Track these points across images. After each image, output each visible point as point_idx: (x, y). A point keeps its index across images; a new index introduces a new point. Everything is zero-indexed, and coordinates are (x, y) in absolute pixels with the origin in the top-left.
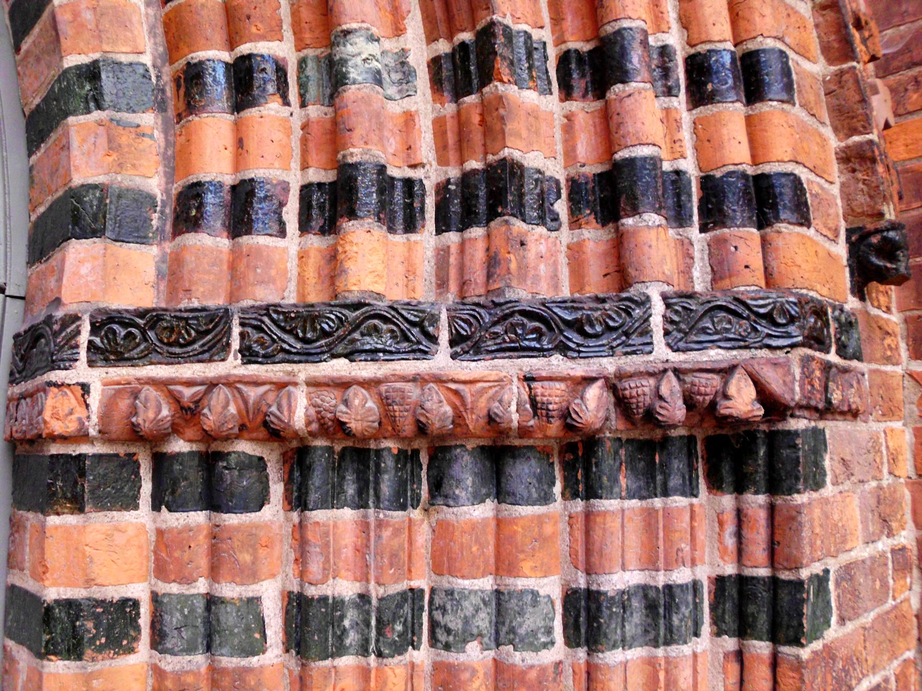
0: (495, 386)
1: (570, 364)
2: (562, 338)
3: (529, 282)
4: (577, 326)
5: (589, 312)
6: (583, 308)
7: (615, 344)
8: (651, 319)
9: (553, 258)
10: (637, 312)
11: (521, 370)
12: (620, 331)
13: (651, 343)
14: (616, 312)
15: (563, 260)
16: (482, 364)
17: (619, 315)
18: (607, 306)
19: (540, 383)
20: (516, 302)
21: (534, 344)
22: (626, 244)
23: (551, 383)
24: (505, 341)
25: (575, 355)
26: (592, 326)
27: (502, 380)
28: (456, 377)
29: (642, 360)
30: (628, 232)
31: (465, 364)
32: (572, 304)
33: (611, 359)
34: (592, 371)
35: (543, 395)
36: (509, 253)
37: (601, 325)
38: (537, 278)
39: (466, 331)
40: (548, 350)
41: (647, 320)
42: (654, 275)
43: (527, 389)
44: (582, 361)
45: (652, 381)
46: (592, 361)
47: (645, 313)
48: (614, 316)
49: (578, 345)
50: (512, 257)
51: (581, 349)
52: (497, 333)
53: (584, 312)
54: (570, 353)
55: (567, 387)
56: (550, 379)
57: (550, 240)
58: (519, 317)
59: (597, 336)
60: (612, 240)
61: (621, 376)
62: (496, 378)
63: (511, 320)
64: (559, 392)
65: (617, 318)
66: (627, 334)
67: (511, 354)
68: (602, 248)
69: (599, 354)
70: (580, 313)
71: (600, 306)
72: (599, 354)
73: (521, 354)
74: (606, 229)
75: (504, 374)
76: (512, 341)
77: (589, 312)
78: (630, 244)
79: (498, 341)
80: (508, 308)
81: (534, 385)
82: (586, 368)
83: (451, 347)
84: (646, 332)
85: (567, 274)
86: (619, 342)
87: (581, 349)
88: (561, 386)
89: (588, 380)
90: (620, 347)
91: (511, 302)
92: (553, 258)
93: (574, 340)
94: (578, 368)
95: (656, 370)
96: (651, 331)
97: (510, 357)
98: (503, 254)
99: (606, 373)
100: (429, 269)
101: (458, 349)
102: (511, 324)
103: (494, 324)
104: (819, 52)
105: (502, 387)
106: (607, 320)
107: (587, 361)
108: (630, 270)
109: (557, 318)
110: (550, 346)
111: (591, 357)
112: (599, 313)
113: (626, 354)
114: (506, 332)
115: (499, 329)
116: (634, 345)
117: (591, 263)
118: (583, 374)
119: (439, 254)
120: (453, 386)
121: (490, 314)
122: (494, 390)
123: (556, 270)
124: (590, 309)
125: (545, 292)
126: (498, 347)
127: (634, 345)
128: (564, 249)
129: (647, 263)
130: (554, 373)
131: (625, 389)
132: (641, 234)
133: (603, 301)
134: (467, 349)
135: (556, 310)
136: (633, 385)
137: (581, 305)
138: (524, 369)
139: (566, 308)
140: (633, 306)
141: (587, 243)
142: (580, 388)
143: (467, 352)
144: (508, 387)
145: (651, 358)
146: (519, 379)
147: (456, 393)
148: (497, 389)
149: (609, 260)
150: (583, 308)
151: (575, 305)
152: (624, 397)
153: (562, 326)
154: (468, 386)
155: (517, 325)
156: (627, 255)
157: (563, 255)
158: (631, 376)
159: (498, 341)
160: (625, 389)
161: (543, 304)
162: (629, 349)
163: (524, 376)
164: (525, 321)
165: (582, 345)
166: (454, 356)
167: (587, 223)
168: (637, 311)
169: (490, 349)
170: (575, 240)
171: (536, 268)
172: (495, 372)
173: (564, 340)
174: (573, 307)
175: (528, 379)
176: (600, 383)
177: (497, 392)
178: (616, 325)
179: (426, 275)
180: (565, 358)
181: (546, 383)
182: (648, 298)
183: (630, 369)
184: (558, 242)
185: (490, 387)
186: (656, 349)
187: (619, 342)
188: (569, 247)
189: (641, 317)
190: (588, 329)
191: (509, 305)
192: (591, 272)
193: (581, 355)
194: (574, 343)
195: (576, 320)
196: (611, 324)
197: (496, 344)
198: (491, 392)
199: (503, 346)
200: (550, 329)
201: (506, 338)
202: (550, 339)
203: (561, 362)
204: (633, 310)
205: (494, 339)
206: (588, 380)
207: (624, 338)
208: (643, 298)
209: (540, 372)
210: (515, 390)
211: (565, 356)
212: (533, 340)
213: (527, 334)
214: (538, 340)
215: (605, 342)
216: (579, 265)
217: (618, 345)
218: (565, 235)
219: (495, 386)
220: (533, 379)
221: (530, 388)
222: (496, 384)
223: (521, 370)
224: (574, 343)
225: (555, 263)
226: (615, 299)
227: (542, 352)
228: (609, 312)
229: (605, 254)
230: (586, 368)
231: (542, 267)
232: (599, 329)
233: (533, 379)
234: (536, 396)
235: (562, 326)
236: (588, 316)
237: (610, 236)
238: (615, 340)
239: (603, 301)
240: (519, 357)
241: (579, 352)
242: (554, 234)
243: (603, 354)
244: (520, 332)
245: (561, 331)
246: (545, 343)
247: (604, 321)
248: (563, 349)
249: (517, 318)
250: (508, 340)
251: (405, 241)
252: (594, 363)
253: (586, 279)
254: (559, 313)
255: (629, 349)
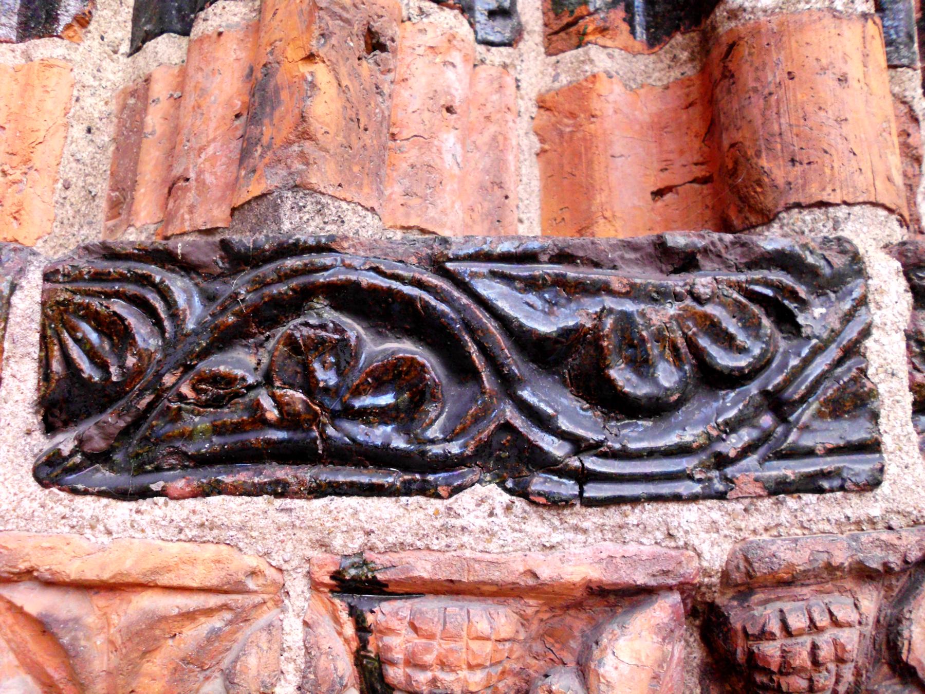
0: (209, 612)
1: (539, 526)
2: (510, 414)
3: (395, 190)
4: (576, 361)
5: (629, 306)
6: (604, 289)
7: (732, 444)
8: (869, 343)
9: (492, 129)
10: (817, 317)
11: (324, 545)
12: (753, 388)
13: (871, 447)
14: (739, 311)
15: (523, 139)
16: (154, 510)
17: (751, 326)
18: (703, 283)
19: (403, 607)
20: (320, 248)
21: (380, 434)
22: (748, 77)
23: (454, 608)
24: (259, 420)
25: (569, 488)
26: (641, 365)
27: (238, 589)
28: (46, 564)
29: (836, 514)
30: (756, 31)
31: (88, 506)
32: (557, 269)
33: (712, 510)
34: (633, 561)
35: (412, 662)
36: (310, 58)
37: (678, 359)
38: (427, 176)
39: (103, 366)
40: (447, 463)
41: (852, 350)
42: (861, 181)
43: (349, 630)
44: (592, 518)
45: (870, 601)
46: (634, 515)
47: (848, 318)
48: (732, 326)
49: (579, 446)
50: (321, 74)
51: (592, 463)
52: (228, 380)
53: (609, 302)
54: (539, 483)
55: (525, 620)
56: (451, 589)
57: (483, 72)
58: (330, 315)
59: (657, 409)
60: (684, 82)
61: (749, 579)
62: (213, 580)
63: (293, 326)
64: (488, 646)
65: (741, 338)
66: (778, 404)
67: (284, 473)
68: (648, 108)
69: (665, 489)
70: (592, 306)
71: (676, 283)
72: (665, 489)
73: (327, 474)
74: (664, 53)
75: (252, 561)
76: (289, 419)
77: (629, 306)
78: (761, 73)
79: (230, 415)
80: (283, 277)
81: (385, 613)
82: (611, 548)
83: (50, 428)
84: (856, 401)
85: (536, 185)
86: (746, 435)
87: (592, 463)
88: (496, 621)
89: (616, 598)
90: (752, 460)
91: (297, 249)
92: (492, 129)
93: (564, 424)
94: (577, 548)
95: (895, 561)
96: (873, 394)
97: (279, 490)
98: (293, 68)
99: (690, 569)
100: (86, 152)
101: (66, 442)
102: (290, 341)
103: (223, 339)
104: (561, 325)
105: (242, 617)
106: (704, 342)
107: (613, 516)
108: (764, 162)
109: (492, 325)
110: (454, 448)
111: (634, 501)
112: (672, 309)
113: (780, 489)
114: (268, 380)
115: (241, 363)
116: (810, 453)
117: (617, 149)
118: (596, 574)
119: (124, 107)
120: (33, 600)
121: (209, 298)
122: (206, 626)
123: (499, 164)
124: (634, 292)
125: (456, 221)
126: (230, 440)
127: (810, 453)
128: (527, 106)
129: (833, 138)
130: (468, 564)
131: (765, 635)
132: (810, 36)
133: (686, 261)
134: (99, 444)
135: (491, 290)
136: (797, 621)
137: (595, 275)
138: (338, 542)
139: (532, 284)
140: (802, 291)
141: (602, 86)
142: (578, 623)
143: (103, 458)
144: (268, 615)
145: (871, 506)
146: (315, 586)
147: (43, 627)
148: (217, 622)
149: (671, 144)
150: (604, 289)
151: (571, 273)
152: (754, 662)
153: (515, 363)
154: (101, 601)
155: (319, 346)
156: (755, 113)
157: (524, 124)
158: (787, 581)
159: (230, 415)
160: (765, 635)
161: (437, 265)
162: (790, 470)
163: (337, 576)
164: (354, 329)
165: (594, 448)
166: (51, 471)
167: (603, 31)
168: (818, 311)
169: (191, 449)
170: (564, 80)
171: (425, 140)
172: (210, 551)
173: (519, 422)
174: (560, 282)
175: (357, 586)
176: (663, 610)
177: (214, 636)
178: (742, 362)
179: (69, 170)
180: (520, 504)
181: (430, 606)
182: (856, 266)
183: (793, 555)
184: (509, 81)
185: (189, 616)
186: (891, 470)
187: (746, 435)
188: (542, 105)
189: (835, 335)
190: (621, 375)
191: (291, 263)
192: (615, 177)
193: (592, 491)
194: (564, 436)
195: (571, 338)
196: (724, 359)
197: (219, 430)
198: (194, 634)
199: (253, 437)
200: (461, 370)
201: (267, 403)
202: (456, 417)
203: (502, 519)
204: (804, 304)
205: (217, 402)
206: (616, 598)
207: (767, 420)
208: (839, 261)
209: (407, 557)
210: (294, 634)
211: (521, 492)
212: (383, 415)
213: (357, 392)
214: (405, 416)
215: (689, 436)
216: (577, 155)
217: (745, 452)
218: (534, 68)
219: (209, 612)
220: (377, 589)
221: (362, 628)
222: (213, 601)
223: (324, 545)
224: (564, 436)
225: (498, 145)
226: (732, 257)
227: (420, 473)
228: (709, 309)
229: (659, 127)
230: (611, 548)
231: (449, 141)
232: (667, 376)
233: (377, 589)
234: (382, 661)
235: (515, 363)
236: (625, 319)
237: (675, 74)
238: (732, 426)
239: (686, 261)
240: (318, 491)
241: (583, 477)
242: (498, 55)
243: (684, 488)
244: (326, 376)
245: (509, 385)
246: (434, 432)
247: (691, 344)
248: (513, 461)
249: (324, 313)
250: (273, 414)
251: (20, 61)
252: (644, 528)
253: (600, 198)
254: (503, 305)
255: (790, 470)
